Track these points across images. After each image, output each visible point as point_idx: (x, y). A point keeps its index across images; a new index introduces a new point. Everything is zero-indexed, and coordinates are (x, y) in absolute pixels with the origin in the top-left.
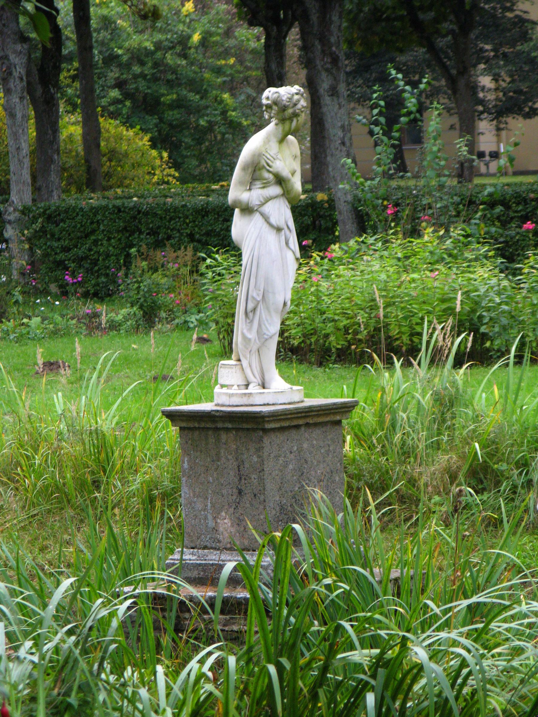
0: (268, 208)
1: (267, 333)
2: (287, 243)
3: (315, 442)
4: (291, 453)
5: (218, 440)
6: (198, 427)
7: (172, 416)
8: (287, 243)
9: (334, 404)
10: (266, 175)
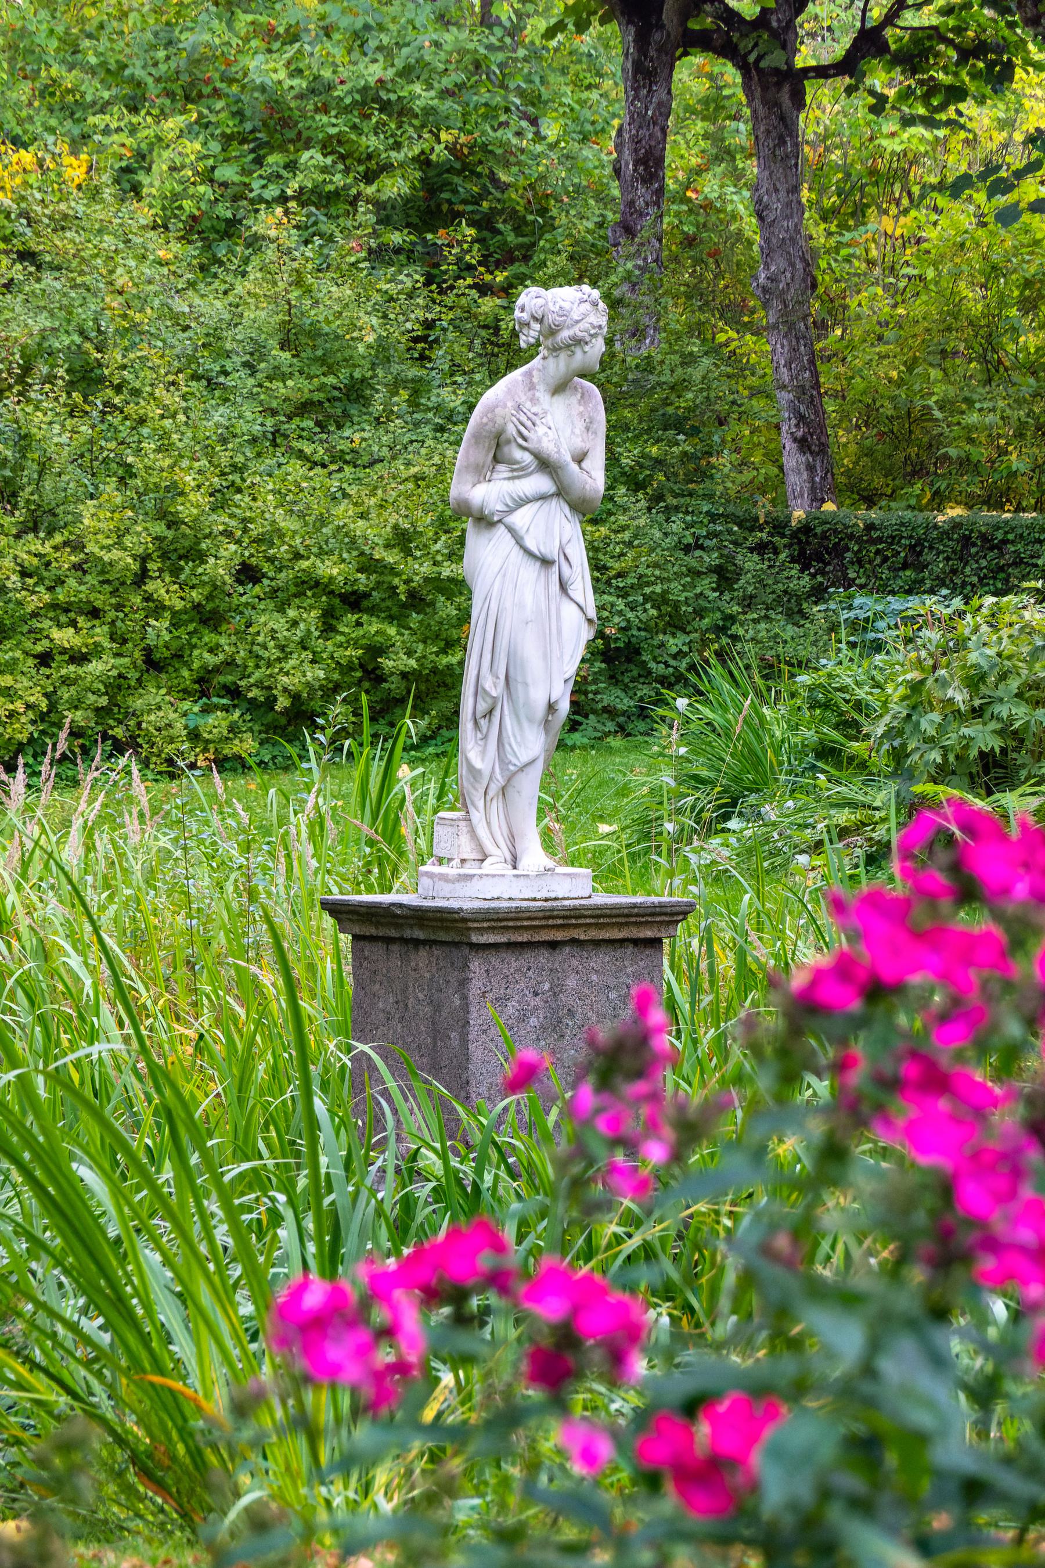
0: (520, 519)
1: (514, 761)
2: (563, 587)
3: (594, 977)
4: (536, 994)
6: (384, 932)
8: (563, 587)
9: (635, 906)
10: (518, 454)
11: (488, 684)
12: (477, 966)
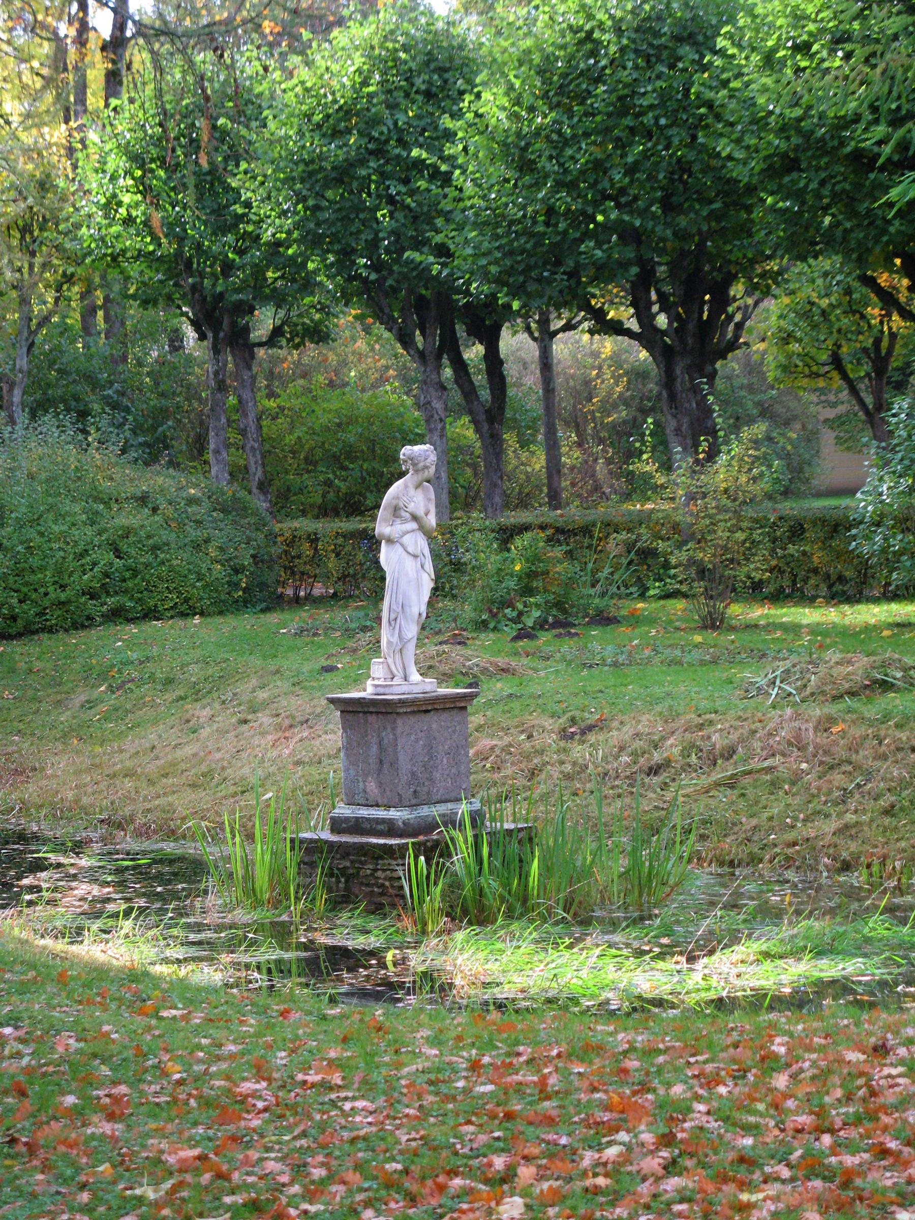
5: (366, 721)
6: (356, 712)
7: (332, 701)
11: (394, 607)
12: (399, 722)
